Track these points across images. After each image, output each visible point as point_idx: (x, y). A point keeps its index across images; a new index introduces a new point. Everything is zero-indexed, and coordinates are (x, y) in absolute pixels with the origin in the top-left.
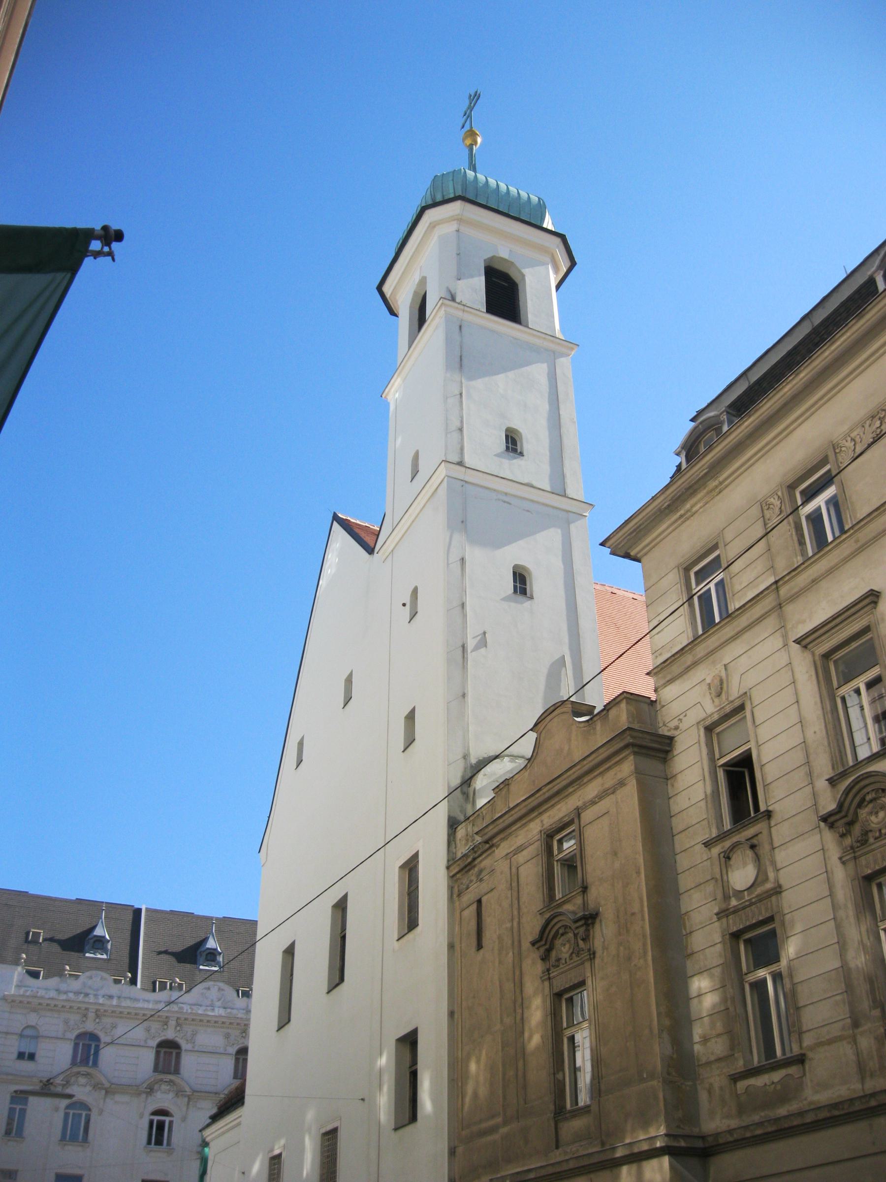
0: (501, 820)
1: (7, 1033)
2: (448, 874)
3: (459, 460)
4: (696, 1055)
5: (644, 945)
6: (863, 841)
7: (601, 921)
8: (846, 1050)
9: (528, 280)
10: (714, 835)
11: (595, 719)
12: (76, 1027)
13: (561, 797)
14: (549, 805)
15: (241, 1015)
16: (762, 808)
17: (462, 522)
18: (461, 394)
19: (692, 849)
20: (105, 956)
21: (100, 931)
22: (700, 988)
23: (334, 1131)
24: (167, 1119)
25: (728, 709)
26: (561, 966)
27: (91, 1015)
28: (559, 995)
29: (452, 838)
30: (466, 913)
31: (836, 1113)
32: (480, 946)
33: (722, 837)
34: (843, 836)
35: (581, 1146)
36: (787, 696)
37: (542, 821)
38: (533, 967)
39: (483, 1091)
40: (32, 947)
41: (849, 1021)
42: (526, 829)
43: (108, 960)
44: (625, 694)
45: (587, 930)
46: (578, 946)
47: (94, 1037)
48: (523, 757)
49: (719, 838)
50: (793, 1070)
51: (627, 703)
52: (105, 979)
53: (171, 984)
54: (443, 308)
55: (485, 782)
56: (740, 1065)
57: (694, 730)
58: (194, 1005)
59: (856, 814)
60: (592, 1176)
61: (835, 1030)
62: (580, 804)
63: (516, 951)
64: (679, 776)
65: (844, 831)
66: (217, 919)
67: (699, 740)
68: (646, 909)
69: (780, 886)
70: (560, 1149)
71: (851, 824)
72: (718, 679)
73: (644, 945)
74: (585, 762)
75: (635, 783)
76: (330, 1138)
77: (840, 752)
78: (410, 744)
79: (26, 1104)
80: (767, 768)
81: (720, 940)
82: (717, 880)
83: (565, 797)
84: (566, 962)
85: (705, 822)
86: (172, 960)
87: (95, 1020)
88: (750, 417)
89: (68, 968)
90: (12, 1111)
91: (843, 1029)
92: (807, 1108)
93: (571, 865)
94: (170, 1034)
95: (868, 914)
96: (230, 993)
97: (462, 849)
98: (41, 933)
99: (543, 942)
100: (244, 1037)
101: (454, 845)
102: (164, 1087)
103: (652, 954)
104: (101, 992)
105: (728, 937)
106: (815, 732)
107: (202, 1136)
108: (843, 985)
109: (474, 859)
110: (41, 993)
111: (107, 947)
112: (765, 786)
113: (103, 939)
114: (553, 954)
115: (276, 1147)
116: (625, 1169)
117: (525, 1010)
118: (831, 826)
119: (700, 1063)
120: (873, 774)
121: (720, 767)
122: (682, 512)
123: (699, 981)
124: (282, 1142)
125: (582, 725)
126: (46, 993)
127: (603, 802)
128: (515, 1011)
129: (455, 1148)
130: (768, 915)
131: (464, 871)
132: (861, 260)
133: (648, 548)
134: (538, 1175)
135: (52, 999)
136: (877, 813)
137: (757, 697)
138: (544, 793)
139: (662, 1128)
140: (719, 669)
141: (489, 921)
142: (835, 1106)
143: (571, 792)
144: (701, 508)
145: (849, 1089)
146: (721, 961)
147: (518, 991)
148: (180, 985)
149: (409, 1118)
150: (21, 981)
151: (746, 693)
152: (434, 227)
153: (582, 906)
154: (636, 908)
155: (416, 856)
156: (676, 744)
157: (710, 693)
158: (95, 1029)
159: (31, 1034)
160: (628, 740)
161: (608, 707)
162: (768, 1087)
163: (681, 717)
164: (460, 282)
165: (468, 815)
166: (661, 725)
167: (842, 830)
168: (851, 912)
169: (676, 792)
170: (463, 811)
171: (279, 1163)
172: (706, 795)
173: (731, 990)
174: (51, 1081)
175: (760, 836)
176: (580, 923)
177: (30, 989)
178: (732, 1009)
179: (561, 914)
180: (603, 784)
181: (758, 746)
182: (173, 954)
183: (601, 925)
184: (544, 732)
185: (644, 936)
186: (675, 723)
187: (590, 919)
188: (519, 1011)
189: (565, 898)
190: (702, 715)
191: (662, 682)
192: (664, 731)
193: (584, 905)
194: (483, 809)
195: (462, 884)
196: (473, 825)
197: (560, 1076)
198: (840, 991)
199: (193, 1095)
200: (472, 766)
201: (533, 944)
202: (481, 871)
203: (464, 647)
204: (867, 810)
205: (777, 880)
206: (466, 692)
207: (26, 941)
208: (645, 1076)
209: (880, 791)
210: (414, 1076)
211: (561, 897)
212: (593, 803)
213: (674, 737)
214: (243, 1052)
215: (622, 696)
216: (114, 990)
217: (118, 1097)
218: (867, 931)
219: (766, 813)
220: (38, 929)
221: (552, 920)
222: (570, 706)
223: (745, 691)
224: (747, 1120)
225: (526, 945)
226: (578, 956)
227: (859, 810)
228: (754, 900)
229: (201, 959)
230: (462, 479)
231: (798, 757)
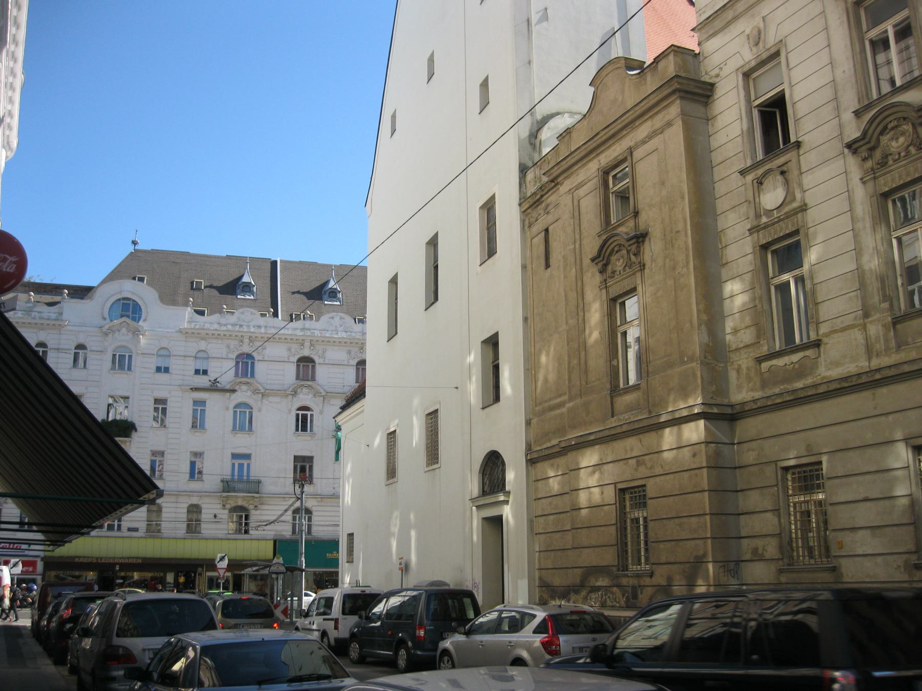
0: (565, 162)
1: (185, 356)
2: (520, 210)
4: (727, 343)
5: (687, 256)
6: (883, 164)
7: (650, 239)
8: (857, 336)
10: (749, 165)
11: (645, 71)
13: (616, 139)
15: (359, 336)
16: (793, 139)
19: (729, 177)
20: (252, 297)
21: (246, 279)
22: (732, 291)
23: (436, 412)
24: (309, 413)
25: (764, 56)
26: (616, 277)
27: (246, 340)
28: (614, 300)
29: (523, 180)
30: (536, 240)
31: (846, 385)
32: (547, 266)
33: (755, 166)
34: (865, 159)
35: (633, 414)
36: (821, 40)
37: (599, 161)
38: (593, 278)
39: (552, 377)
40: (196, 293)
41: (861, 312)
42: (585, 168)
44: (673, 47)
45: (638, 247)
46: (630, 260)
47: (250, 356)
48: (580, 113)
49: (752, 167)
50: (809, 353)
51: (674, 55)
52: (254, 314)
53: (304, 316)
55: (549, 135)
56: (764, 350)
57: (734, 76)
58: (323, 330)
59: (878, 141)
60: (641, 436)
61: (849, 320)
62: (632, 144)
63: (578, 267)
64: (719, 117)
65: (866, 155)
66: (335, 266)
67: (737, 85)
68: (689, 227)
69: (806, 205)
70: (615, 418)
71: (872, 149)
72: (757, 29)
73: (687, 256)
74: (637, 108)
75: (681, 123)
76: (433, 416)
77: (866, 88)
78: (485, 107)
79: (205, 406)
80: (798, 105)
81: (751, 251)
82: (750, 202)
84: (620, 274)
85: (741, 154)
86: (304, 298)
89: (225, 307)
90: (195, 411)
91: (855, 318)
92: (820, 382)
93: (623, 197)
94: (306, 353)
95: (883, 226)
96: (349, 320)
97: (531, 189)
99: (601, 259)
100: (362, 353)
101: (524, 187)
102: (305, 390)
103: (694, 264)
104: (252, 324)
105: (758, 248)
106: (844, 72)
107: (335, 421)
108: (858, 284)
109: (542, 196)
110: (207, 326)
111: (253, 290)
112: (796, 121)
114: (610, 268)
115: (391, 426)
116: (667, 430)
117: (586, 314)
118: (855, 152)
119: (731, 349)
120: (897, 104)
121: (755, 107)
123: (732, 285)
124: (396, 422)
125: (635, 77)
127: (652, 141)
128: (578, 314)
129: (530, 420)
130: (794, 229)
131: (533, 207)
134: (597, 437)
135: (216, 330)
136: (897, 139)
137: (791, 43)
138: (602, 137)
139: (699, 399)
140: (758, 21)
141: (554, 245)
142: (845, 379)
143: (625, 135)
145: (857, 366)
147: (580, 298)
148: (311, 317)
149: (493, 399)
150: (191, 318)
151: (781, 40)
153: (634, 228)
154: (680, 226)
155: (493, 198)
156: (717, 89)
157: (749, 43)
159: (202, 356)
160: (676, 86)
161: (657, 60)
162: (788, 367)
163: (721, 66)
165: (535, 162)
166: (703, 74)
167: (865, 154)
168: (868, 224)
169: (715, 131)
170: (531, 158)
171: (394, 437)
172: (742, 132)
173: (759, 292)
174: (218, 380)
175: (789, 164)
176: (633, 241)
178: (759, 306)
179: (617, 235)
180: (652, 126)
181: (791, 86)
182: (304, 294)
183: (650, 242)
184: (600, 87)
185: (687, 249)
186: (716, 71)
187: (640, 238)
188: (581, 314)
189: (619, 222)
190: (741, 63)
191: (705, 36)
192: (706, 79)
193: (636, 227)
194: (548, 155)
195: (532, 217)
196: (540, 169)
197: (615, 363)
198: (855, 289)
199: (326, 395)
200: (538, 122)
201: (593, 260)
202: (548, 206)
203: (528, 21)
204: (888, 136)
205: (803, 200)
206: (531, 59)
207: (192, 288)
208: (686, 360)
209: (902, 120)
210: (496, 368)
211: (615, 221)
212: (644, 142)
213: (715, 84)
214: (362, 363)
215: (671, 49)
216: (262, 321)
217: (271, 399)
218: (882, 239)
219: (796, 143)
220: (200, 279)
221: (608, 240)
222: (624, 62)
223: (780, 39)
224: (769, 392)
225: (587, 261)
226: (630, 268)
227: (881, 137)
228: (782, 217)
229: (325, 297)
231: (828, 94)
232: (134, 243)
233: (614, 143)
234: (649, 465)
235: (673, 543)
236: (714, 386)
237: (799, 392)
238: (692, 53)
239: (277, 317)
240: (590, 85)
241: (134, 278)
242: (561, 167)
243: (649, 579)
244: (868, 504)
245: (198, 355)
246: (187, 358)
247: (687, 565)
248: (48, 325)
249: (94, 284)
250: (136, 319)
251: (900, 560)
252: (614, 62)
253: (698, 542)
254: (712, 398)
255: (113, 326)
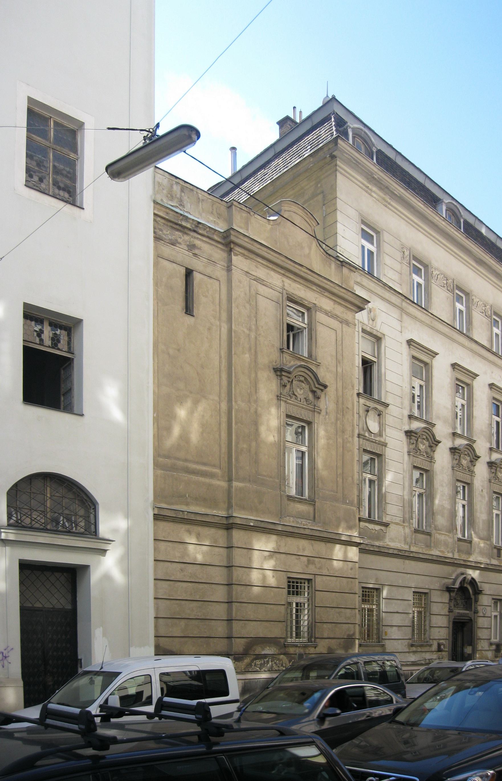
14: (294, 278)
50: (383, 528)
74: (337, 288)
83: (306, 286)
88: (424, 205)
122: (370, 187)
132: (412, 162)
144: (375, 198)
233: (301, 283)
234: (318, 566)
235: (333, 624)
237: (382, 548)
242: (252, 245)
243: (313, 649)
244: (398, 614)
247: (343, 640)
251: (406, 642)
252: (307, 214)
253: (350, 625)
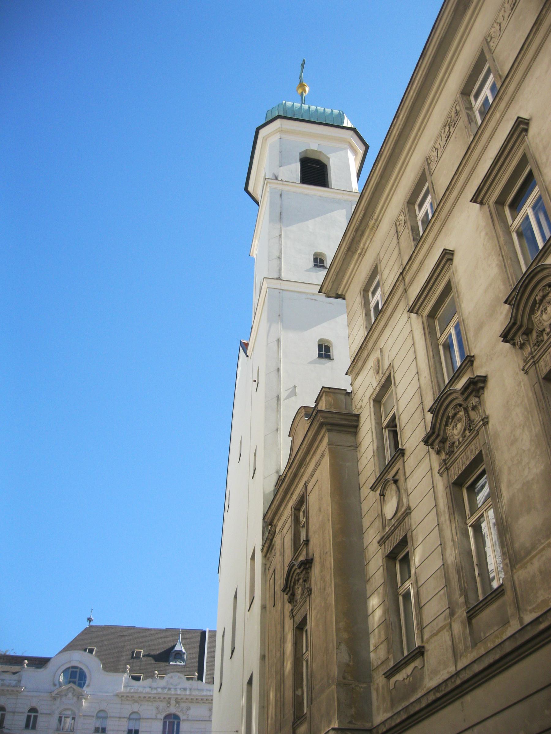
1: (120, 718)
3: (278, 277)
4: (371, 661)
8: (445, 636)
9: (331, 161)
12: (164, 710)
13: (299, 478)
16: (400, 447)
17: (279, 315)
18: (280, 236)
20: (182, 664)
27: (173, 702)
31: (439, 695)
40: (136, 662)
43: (184, 666)
47: (176, 717)
50: (417, 663)
54: (268, 185)
63: (282, 601)
64: (362, 443)
87: (176, 705)
91: (445, 619)
98: (141, 651)
99: (288, 589)
104: (179, 687)
106: (425, 377)
110: (141, 689)
111: (183, 658)
113: (180, 652)
122: (359, 251)
126: (144, 690)
133: (347, 286)
135: (148, 693)
143: (303, 472)
145: (448, 672)
146: (383, 581)
152: (266, 139)
158: (176, 711)
164: (281, 168)
177: (133, 688)
183: (314, 568)
192: (356, 412)
197: (299, 692)
203: (278, 398)
206: (279, 427)
207: (132, 657)
209: (458, 407)
213: (360, 414)
216: (188, 684)
220: (140, 649)
227: (446, 428)
230: (279, 288)
232: (90, 620)
236: (353, 710)
238: (344, 392)
239: (202, 680)
240: (289, 436)
241: (85, 650)
245: (132, 716)
246: (122, 720)
248: (8, 691)
249: (52, 657)
250: (81, 685)
252: (299, 412)
254: (350, 722)
255: (61, 691)
